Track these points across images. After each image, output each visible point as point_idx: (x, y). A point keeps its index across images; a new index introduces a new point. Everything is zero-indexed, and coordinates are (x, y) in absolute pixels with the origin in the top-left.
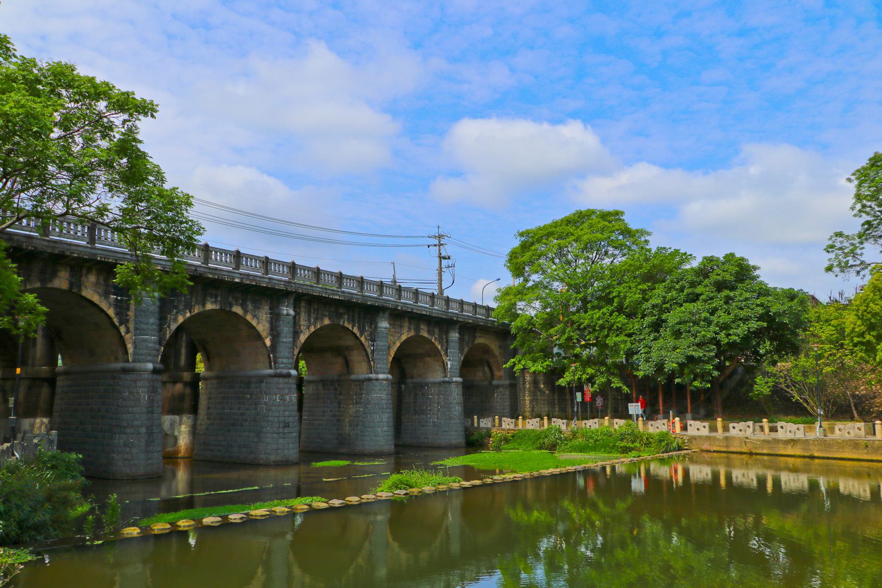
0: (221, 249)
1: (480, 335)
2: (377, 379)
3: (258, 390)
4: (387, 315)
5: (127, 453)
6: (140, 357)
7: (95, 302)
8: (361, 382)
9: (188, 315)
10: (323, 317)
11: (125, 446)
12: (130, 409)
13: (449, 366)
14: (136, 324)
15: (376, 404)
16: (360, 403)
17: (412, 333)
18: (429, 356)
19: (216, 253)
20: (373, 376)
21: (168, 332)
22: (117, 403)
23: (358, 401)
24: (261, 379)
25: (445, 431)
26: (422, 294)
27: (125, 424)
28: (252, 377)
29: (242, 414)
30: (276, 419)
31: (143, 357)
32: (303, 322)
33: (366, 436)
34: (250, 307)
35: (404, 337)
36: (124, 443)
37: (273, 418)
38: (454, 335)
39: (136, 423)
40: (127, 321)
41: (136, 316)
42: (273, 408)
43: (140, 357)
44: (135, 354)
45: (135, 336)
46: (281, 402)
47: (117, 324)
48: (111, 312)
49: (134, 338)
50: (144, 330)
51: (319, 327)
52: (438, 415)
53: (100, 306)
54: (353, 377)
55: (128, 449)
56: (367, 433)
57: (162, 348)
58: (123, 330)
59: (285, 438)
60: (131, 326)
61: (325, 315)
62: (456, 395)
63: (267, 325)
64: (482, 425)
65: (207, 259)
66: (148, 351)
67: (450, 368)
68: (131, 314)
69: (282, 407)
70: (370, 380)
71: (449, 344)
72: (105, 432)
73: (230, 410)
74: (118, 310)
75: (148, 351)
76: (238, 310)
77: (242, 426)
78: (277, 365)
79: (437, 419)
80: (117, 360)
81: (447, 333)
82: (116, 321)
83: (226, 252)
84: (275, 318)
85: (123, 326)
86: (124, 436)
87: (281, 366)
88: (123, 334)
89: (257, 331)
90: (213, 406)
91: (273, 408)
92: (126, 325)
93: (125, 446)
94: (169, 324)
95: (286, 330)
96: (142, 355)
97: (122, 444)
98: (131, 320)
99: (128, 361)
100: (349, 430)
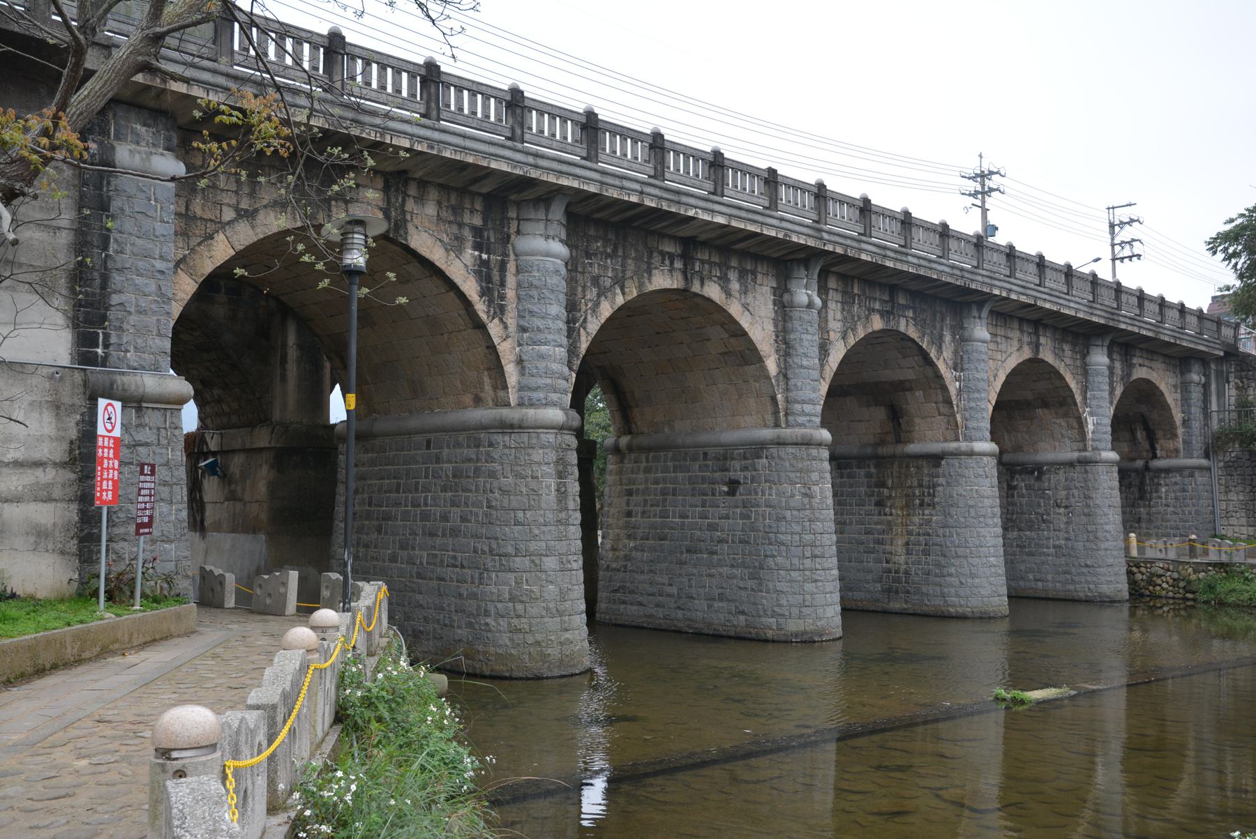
0: (389, 56)
1: (1141, 361)
2: (971, 454)
3: (749, 474)
4: (557, 212)
5: (519, 616)
6: (535, 395)
7: (438, 264)
8: (936, 459)
9: (620, 300)
10: (869, 314)
11: (513, 599)
12: (520, 514)
13: (1091, 427)
14: (521, 316)
15: (971, 506)
16: (932, 505)
17: (1027, 354)
18: (1046, 405)
19: (367, 63)
20: (963, 446)
21: (583, 338)
22: (488, 501)
23: (926, 499)
24: (757, 449)
25: (1087, 566)
26: (788, 186)
27: (510, 550)
28: (735, 445)
29: (712, 527)
30: (797, 538)
31: (542, 395)
32: (835, 325)
33: (950, 575)
34: (735, 286)
35: (1012, 363)
36: (510, 593)
37: (789, 537)
38: (538, 243)
39: (533, 546)
40: (502, 309)
41: (519, 298)
42: (788, 513)
43: (535, 395)
44: (521, 388)
45: (520, 345)
46: (806, 500)
47: (483, 316)
48: (470, 287)
49: (518, 349)
50: (539, 330)
51: (862, 336)
52: (1067, 532)
53: (447, 273)
54: (912, 448)
55: (519, 607)
56: (952, 570)
57: (574, 375)
58: (494, 329)
59: (816, 581)
60: (511, 321)
61: (873, 310)
62: (1107, 487)
63: (770, 327)
64: (1150, 554)
65: (432, 109)
66: (549, 381)
67: (1093, 432)
68: (510, 293)
69: (807, 512)
70: (957, 454)
71: (1091, 379)
72: (463, 567)
73: (681, 517)
74: (484, 284)
75: (549, 381)
76: (713, 291)
77: (713, 553)
78: (791, 418)
79: (1068, 539)
80: (478, 401)
81: (1085, 355)
82: (480, 307)
83: (399, 66)
84: (784, 309)
85: (496, 321)
86: (511, 577)
87: (801, 419)
88: (496, 340)
89: (750, 341)
90: (640, 509)
91: (788, 513)
92: (501, 320)
93: (513, 599)
94: (585, 321)
95: (807, 341)
96: (536, 389)
97: (507, 596)
98: (509, 308)
99: (508, 405)
100: (907, 563)
